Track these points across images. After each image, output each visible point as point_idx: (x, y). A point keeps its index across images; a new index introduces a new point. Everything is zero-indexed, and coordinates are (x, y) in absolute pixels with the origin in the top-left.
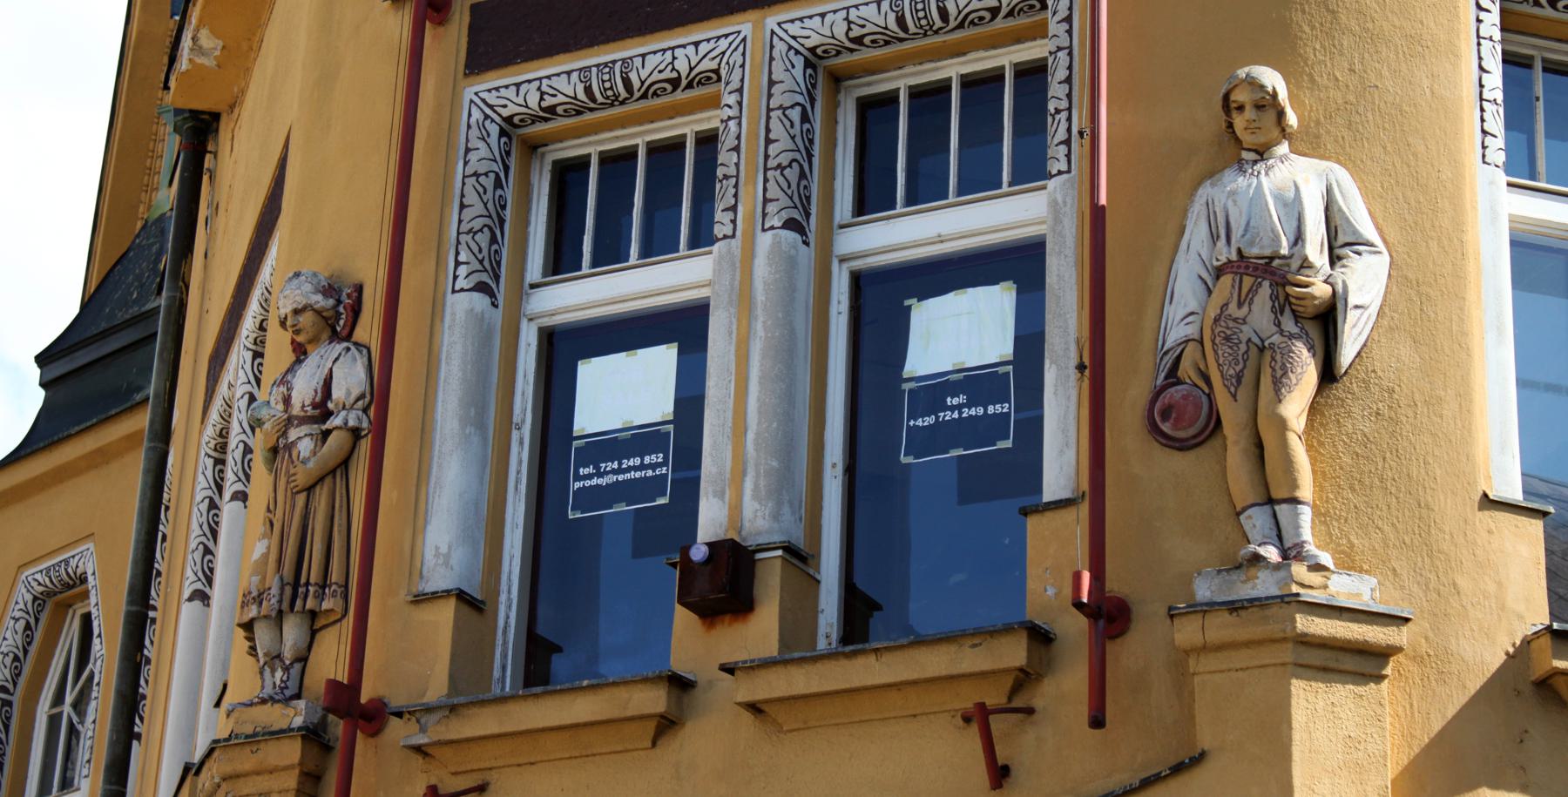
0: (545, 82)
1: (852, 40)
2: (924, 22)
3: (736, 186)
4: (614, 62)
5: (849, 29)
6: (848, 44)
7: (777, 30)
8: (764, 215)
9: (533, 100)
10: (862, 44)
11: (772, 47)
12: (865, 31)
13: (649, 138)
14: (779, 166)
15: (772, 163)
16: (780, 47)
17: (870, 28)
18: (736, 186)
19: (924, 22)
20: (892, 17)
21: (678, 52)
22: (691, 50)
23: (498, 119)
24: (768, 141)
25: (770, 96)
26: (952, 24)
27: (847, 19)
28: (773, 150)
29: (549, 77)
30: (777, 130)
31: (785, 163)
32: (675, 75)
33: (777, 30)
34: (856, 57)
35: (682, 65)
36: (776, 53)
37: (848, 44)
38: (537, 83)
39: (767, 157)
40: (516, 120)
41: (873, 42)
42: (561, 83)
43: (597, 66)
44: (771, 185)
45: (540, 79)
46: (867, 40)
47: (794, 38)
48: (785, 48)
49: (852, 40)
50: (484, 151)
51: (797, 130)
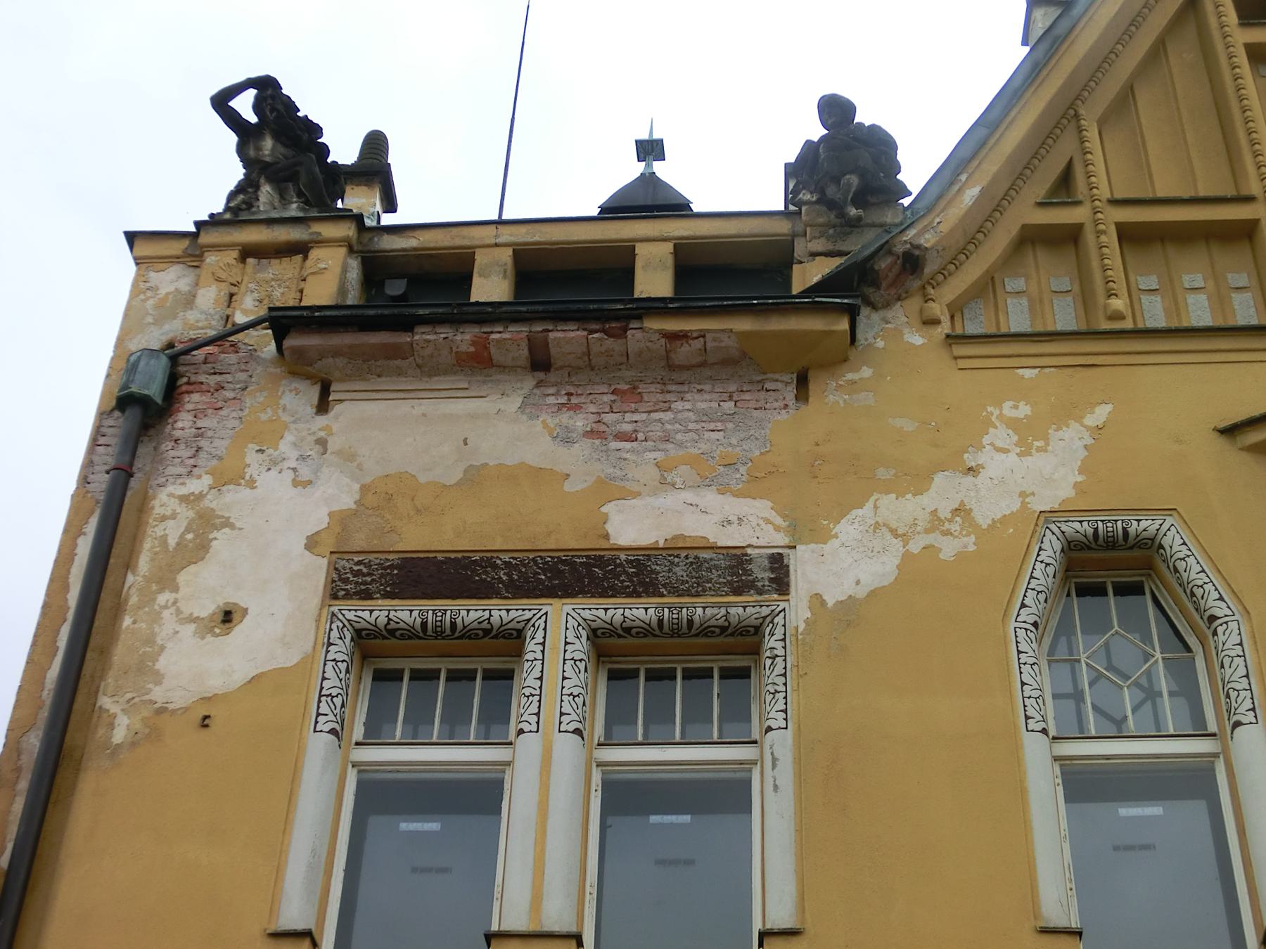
0: (392, 613)
1: (623, 629)
3: (785, 698)
6: (384, 633)
8: (316, 722)
15: (565, 691)
16: (572, 622)
17: (402, 625)
18: (785, 698)
24: (324, 679)
25: (327, 652)
26: (457, 635)
28: (326, 684)
30: (330, 673)
32: (489, 626)
34: (621, 641)
37: (384, 633)
39: (322, 688)
40: (599, 632)
41: (638, 633)
44: (323, 704)
46: (634, 631)
49: (623, 629)
51: (342, 676)
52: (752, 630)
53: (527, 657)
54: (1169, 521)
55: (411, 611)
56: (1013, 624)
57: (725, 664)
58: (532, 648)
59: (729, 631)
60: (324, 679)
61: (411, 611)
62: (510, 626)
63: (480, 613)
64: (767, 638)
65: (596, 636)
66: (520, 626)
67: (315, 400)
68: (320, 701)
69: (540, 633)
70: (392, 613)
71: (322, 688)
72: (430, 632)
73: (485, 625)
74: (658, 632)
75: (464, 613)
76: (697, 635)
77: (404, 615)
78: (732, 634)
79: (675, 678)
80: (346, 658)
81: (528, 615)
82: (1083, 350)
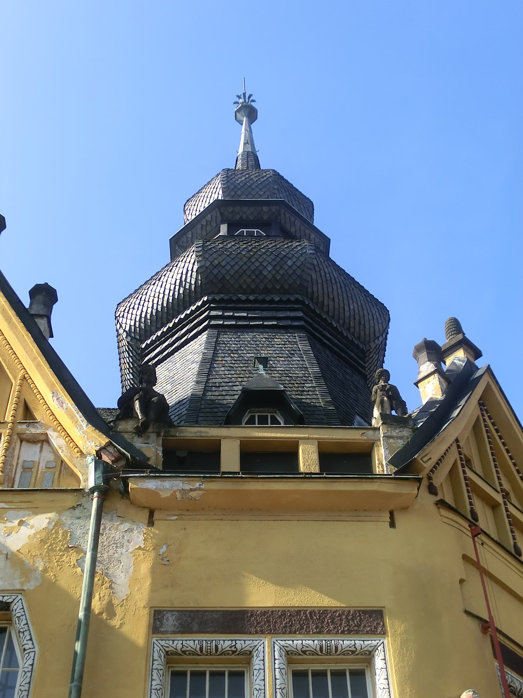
0: (184, 642)
1: (182, 651)
2: (209, 650)
4: (213, 640)
5: (183, 647)
7: (156, 642)
9: (179, 646)
10: (305, 654)
11: (154, 647)
12: (187, 649)
13: (210, 669)
14: (156, 689)
17: (189, 648)
19: (209, 650)
20: (198, 646)
21: (237, 642)
22: (243, 642)
23: (284, 650)
26: (218, 653)
27: (182, 644)
28: (154, 683)
29: (186, 640)
31: (158, 689)
33: (156, 642)
34: (300, 657)
35: (239, 647)
36: (276, 649)
37: (300, 652)
38: (181, 642)
40: (169, 653)
41: (291, 653)
42: (191, 643)
43: (206, 640)
45: (183, 640)
46: (187, 653)
47: (162, 646)
48: (159, 649)
50: (159, 662)
52: (368, 653)
53: (254, 668)
54: (20, 597)
55: (194, 641)
56: (36, 649)
57: (193, 669)
58: (256, 663)
59: (238, 653)
60: (152, 680)
61: (194, 641)
62: (246, 649)
63: (349, 642)
64: (255, 658)
65: (288, 654)
66: (251, 649)
67: (146, 521)
68: (151, 692)
69: (261, 654)
70: (184, 642)
71: (152, 685)
72: (204, 652)
73: (353, 649)
74: (199, 653)
75: (222, 642)
76: (220, 655)
77: (191, 643)
78: (238, 654)
79: (326, 676)
80: (162, 668)
81: (256, 643)
82: (450, 517)
